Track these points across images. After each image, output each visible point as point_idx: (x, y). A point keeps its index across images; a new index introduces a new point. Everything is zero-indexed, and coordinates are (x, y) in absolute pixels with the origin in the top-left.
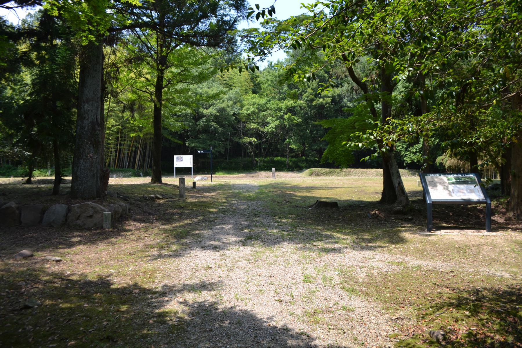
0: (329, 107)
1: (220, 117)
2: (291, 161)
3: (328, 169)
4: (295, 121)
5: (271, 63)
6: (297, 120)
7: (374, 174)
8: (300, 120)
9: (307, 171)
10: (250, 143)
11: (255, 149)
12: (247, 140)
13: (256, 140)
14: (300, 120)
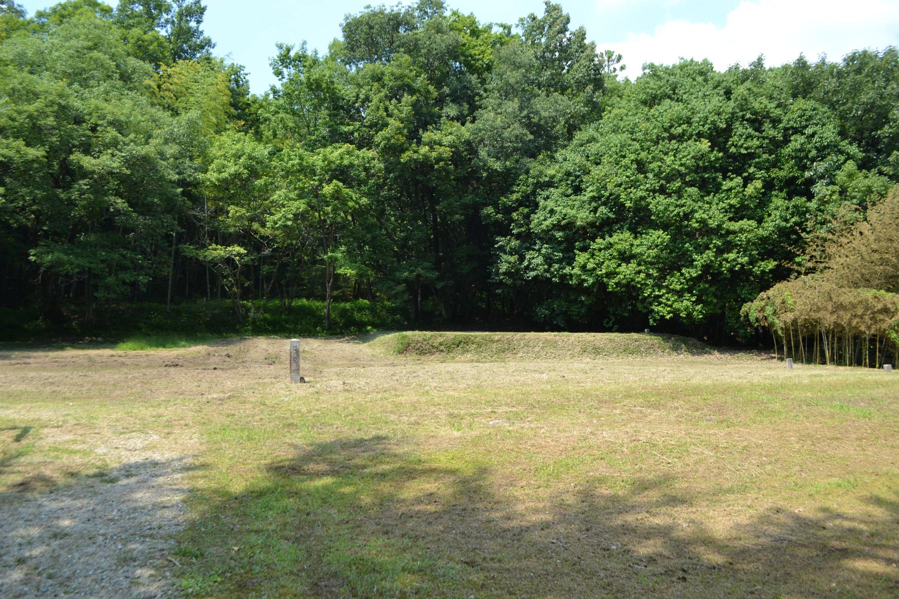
0: (444, 169)
1: (138, 181)
2: (335, 308)
3: (451, 335)
4: (351, 204)
5: (289, 50)
6: (357, 198)
7: (578, 349)
8: (364, 201)
9: (392, 338)
10: (229, 261)
11: (242, 278)
12: (216, 252)
13: (242, 251)
14: (364, 201)
